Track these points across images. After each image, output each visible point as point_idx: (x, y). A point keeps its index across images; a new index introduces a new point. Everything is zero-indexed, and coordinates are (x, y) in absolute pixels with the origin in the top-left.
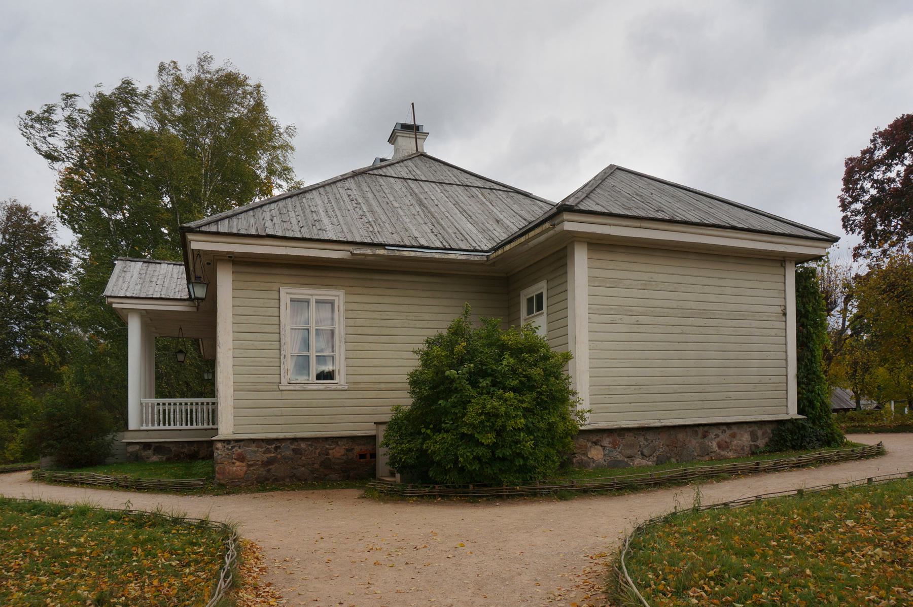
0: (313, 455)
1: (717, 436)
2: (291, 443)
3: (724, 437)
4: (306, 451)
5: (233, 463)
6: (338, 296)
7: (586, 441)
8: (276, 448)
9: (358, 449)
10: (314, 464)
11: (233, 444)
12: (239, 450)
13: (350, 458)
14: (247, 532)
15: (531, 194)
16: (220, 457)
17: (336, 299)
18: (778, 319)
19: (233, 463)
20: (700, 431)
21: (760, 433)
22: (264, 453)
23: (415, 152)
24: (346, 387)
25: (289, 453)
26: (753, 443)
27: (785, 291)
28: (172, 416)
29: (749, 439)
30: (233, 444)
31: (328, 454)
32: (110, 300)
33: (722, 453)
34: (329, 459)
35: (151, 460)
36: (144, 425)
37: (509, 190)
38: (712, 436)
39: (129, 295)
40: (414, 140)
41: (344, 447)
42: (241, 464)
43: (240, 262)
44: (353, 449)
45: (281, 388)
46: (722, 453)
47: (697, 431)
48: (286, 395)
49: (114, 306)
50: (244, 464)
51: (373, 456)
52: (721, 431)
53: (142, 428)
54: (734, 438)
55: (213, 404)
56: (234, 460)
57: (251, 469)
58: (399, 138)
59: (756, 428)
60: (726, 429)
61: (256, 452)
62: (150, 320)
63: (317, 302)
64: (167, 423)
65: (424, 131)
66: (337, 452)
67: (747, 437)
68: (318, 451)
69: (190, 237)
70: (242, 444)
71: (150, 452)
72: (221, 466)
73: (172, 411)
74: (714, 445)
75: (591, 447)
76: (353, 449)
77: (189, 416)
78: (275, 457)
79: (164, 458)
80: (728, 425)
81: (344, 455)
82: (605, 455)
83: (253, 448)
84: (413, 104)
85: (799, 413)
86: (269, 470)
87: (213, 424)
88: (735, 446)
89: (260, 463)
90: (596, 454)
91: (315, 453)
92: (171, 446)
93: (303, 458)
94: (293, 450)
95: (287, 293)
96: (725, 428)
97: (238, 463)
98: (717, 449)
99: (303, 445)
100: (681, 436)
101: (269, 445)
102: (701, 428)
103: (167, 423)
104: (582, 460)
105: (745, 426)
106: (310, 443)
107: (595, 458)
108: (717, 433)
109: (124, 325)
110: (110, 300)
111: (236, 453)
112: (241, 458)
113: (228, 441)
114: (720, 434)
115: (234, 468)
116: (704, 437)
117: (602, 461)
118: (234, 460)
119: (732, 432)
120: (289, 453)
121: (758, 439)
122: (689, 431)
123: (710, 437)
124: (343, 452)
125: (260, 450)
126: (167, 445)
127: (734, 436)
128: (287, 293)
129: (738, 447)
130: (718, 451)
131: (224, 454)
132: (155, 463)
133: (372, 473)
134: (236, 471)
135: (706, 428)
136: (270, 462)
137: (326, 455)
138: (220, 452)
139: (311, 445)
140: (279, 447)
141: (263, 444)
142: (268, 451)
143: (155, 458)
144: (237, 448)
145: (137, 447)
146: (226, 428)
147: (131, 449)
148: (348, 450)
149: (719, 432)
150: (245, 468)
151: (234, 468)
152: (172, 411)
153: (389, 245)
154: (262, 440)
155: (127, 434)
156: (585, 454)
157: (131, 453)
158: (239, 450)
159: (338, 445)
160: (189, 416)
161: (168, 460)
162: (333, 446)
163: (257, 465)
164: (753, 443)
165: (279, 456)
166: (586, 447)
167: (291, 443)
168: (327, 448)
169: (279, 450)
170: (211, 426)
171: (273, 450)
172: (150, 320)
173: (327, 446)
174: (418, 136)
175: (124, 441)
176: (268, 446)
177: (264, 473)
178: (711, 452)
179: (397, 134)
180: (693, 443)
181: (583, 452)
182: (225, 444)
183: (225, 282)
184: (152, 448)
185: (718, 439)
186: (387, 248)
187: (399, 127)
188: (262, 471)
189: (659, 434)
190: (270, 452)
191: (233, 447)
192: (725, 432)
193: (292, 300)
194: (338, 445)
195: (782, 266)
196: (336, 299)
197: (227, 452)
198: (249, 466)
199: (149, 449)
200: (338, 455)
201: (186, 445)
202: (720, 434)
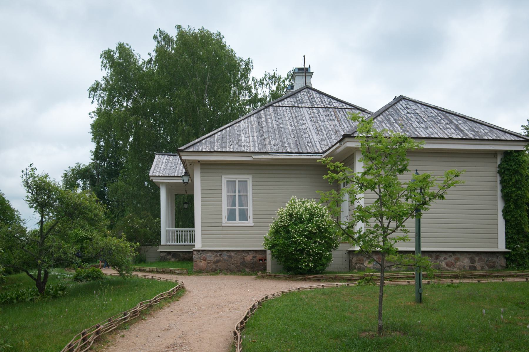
0: (237, 259)
1: (445, 259)
2: (227, 253)
4: (234, 257)
5: (201, 261)
6: (249, 179)
7: (363, 257)
8: (220, 255)
9: (258, 256)
10: (237, 263)
12: (204, 255)
13: (255, 261)
15: (366, 110)
16: (195, 258)
17: (248, 180)
18: (491, 190)
19: (201, 261)
20: (434, 255)
22: (215, 257)
23: (305, 86)
24: (253, 225)
25: (225, 257)
26: (472, 265)
28: (183, 237)
31: (244, 259)
32: (152, 178)
34: (245, 261)
36: (168, 242)
37: (352, 108)
38: (442, 258)
39: (161, 175)
40: (304, 77)
41: (251, 255)
42: (204, 262)
44: (256, 256)
49: (154, 181)
50: (206, 262)
51: (265, 260)
52: (448, 256)
53: (168, 244)
54: (458, 260)
55: (192, 231)
56: (201, 260)
57: (209, 264)
58: (296, 77)
59: (474, 256)
60: (452, 255)
61: (211, 256)
62: (170, 187)
64: (178, 241)
65: (311, 71)
67: (467, 261)
68: (239, 257)
70: (205, 252)
72: (195, 262)
73: (183, 235)
74: (444, 264)
75: (366, 260)
76: (256, 256)
77: (191, 238)
80: (454, 253)
81: (251, 260)
83: (210, 254)
84: (304, 56)
85: (506, 248)
86: (217, 266)
87: (193, 242)
88: (458, 265)
91: (238, 258)
93: (233, 260)
95: (225, 178)
96: (451, 254)
97: (203, 262)
98: (445, 266)
99: (232, 254)
102: (435, 254)
103: (178, 241)
104: (360, 267)
105: (465, 254)
106: (235, 253)
108: (446, 257)
109: (159, 189)
110: (152, 178)
111: (202, 256)
112: (205, 259)
113: (198, 251)
114: (448, 258)
115: (202, 264)
116: (437, 258)
118: (201, 260)
119: (456, 257)
120: (225, 257)
123: (441, 259)
124: (251, 258)
125: (213, 255)
127: (457, 259)
128: (225, 179)
129: (460, 266)
130: (446, 268)
131: (197, 257)
133: (265, 269)
134: (202, 265)
135: (438, 254)
136: (218, 262)
137: (243, 259)
139: (236, 254)
140: (221, 254)
141: (214, 253)
142: (216, 256)
143: (173, 260)
144: (203, 254)
145: (165, 254)
147: (162, 255)
149: (447, 256)
150: (206, 264)
151: (202, 264)
152: (183, 235)
153: (271, 153)
155: (160, 247)
156: (362, 264)
157: (162, 257)
158: (204, 255)
159: (249, 254)
160: (191, 238)
162: (247, 255)
163: (212, 263)
164: (472, 265)
165: (221, 259)
166: (363, 260)
168: (243, 256)
169: (221, 256)
170: (191, 243)
171: (218, 255)
172: (170, 187)
173: (244, 255)
174: (306, 75)
175: (159, 250)
176: (216, 254)
177: (215, 267)
178: (442, 268)
179: (295, 75)
181: (361, 263)
182: (198, 252)
185: (446, 261)
186: (270, 154)
187: (296, 71)
188: (214, 266)
190: (217, 256)
191: (201, 254)
192: (451, 257)
194: (249, 254)
196: (248, 180)
197: (198, 256)
199: (170, 255)
200: (249, 259)
201: (187, 254)
202: (448, 258)
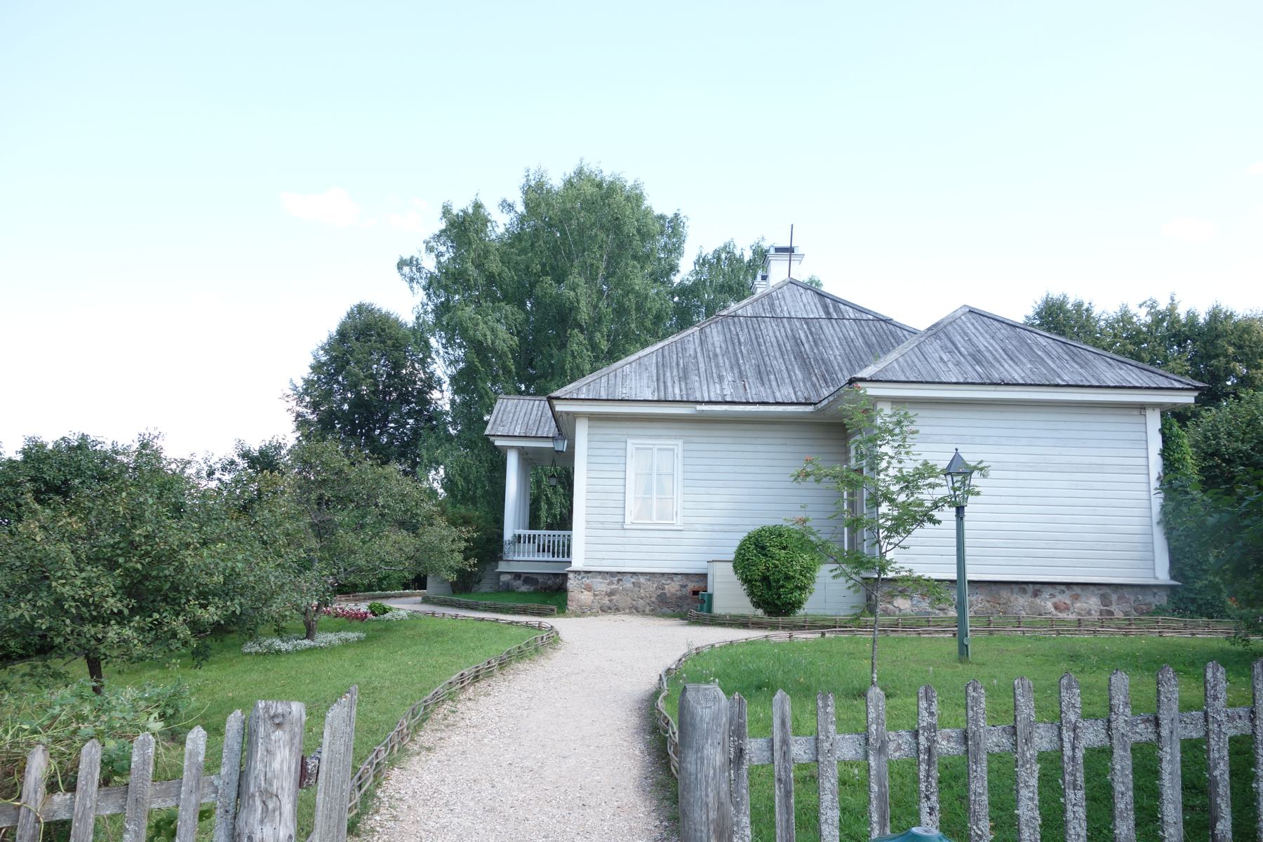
1: (1053, 596)
3: (1064, 598)
6: (678, 445)
9: (692, 586)
10: (651, 597)
11: (582, 574)
12: (588, 581)
14: (557, 627)
17: (675, 447)
21: (1114, 597)
25: (629, 585)
27: (1147, 441)
29: (1100, 603)
30: (582, 574)
33: (1061, 615)
35: (520, 590)
42: (588, 593)
43: (593, 417)
45: (625, 527)
46: (1061, 615)
47: (1024, 589)
48: (629, 533)
55: (569, 536)
60: (1066, 590)
63: (659, 449)
66: (672, 588)
69: (555, 402)
71: (520, 582)
78: (618, 589)
79: (532, 589)
82: (913, 605)
83: (599, 579)
85: (1173, 578)
89: (603, 593)
90: (902, 604)
92: (539, 577)
94: (633, 583)
96: (1063, 587)
97: (586, 592)
99: (642, 580)
100: (1004, 593)
101: (613, 577)
103: (1222, 772)
104: (887, 608)
105: (1092, 588)
107: (902, 607)
112: (589, 588)
117: (908, 611)
120: (629, 585)
121: (1111, 604)
122: (1016, 588)
124: (678, 588)
126: (535, 576)
132: (524, 593)
135: (1037, 587)
136: (611, 594)
138: (572, 583)
139: (649, 580)
141: (608, 576)
142: (611, 583)
143: (524, 588)
146: (579, 561)
148: (682, 586)
154: (607, 573)
158: (588, 581)
161: (536, 591)
167: (631, 577)
180: (1021, 602)
183: (582, 434)
184: (522, 579)
185: (1054, 600)
189: (977, 588)
190: (613, 583)
191: (583, 578)
193: (637, 449)
195: (1141, 414)
197: (578, 582)
198: (595, 595)
200: (673, 590)
202: (1057, 594)
